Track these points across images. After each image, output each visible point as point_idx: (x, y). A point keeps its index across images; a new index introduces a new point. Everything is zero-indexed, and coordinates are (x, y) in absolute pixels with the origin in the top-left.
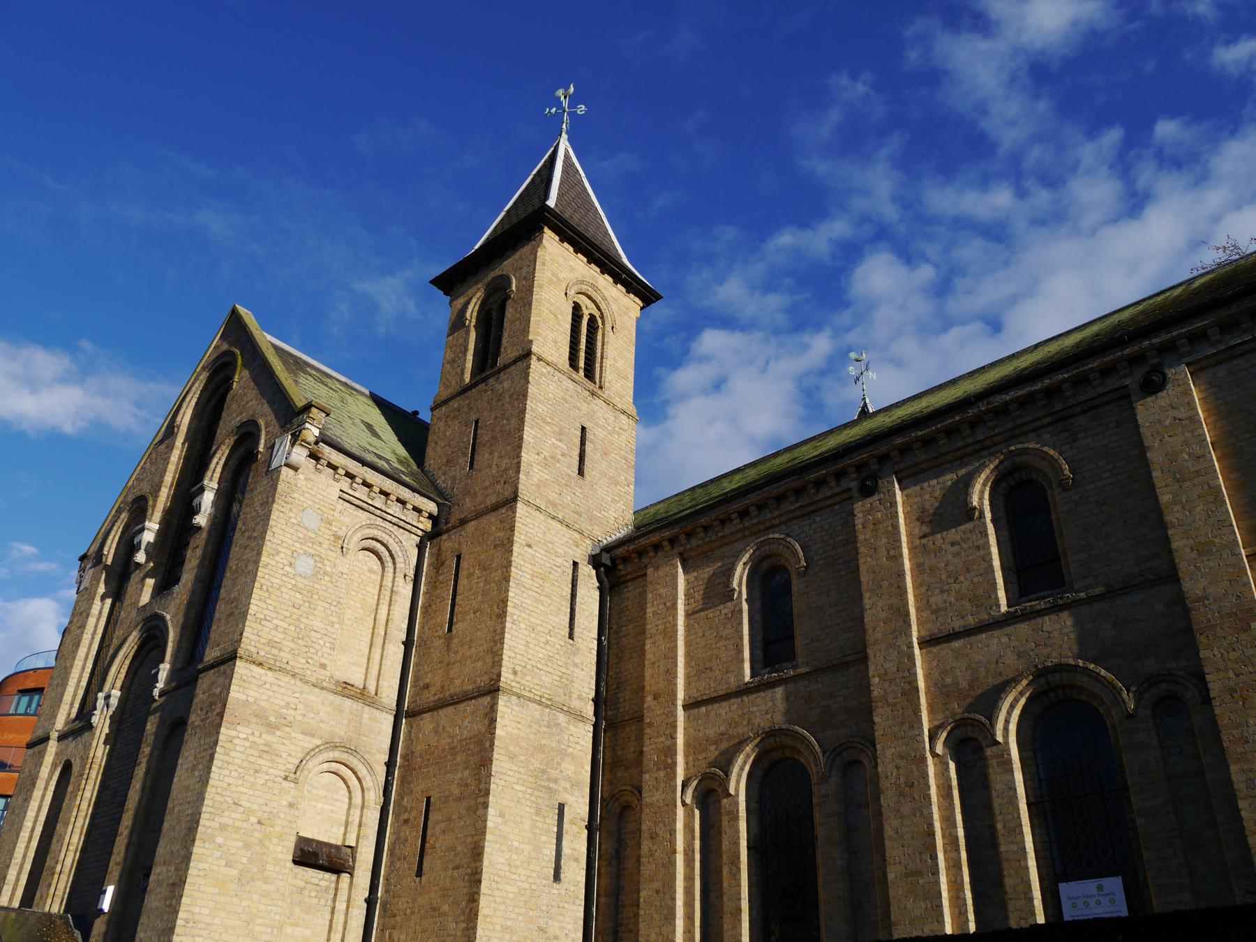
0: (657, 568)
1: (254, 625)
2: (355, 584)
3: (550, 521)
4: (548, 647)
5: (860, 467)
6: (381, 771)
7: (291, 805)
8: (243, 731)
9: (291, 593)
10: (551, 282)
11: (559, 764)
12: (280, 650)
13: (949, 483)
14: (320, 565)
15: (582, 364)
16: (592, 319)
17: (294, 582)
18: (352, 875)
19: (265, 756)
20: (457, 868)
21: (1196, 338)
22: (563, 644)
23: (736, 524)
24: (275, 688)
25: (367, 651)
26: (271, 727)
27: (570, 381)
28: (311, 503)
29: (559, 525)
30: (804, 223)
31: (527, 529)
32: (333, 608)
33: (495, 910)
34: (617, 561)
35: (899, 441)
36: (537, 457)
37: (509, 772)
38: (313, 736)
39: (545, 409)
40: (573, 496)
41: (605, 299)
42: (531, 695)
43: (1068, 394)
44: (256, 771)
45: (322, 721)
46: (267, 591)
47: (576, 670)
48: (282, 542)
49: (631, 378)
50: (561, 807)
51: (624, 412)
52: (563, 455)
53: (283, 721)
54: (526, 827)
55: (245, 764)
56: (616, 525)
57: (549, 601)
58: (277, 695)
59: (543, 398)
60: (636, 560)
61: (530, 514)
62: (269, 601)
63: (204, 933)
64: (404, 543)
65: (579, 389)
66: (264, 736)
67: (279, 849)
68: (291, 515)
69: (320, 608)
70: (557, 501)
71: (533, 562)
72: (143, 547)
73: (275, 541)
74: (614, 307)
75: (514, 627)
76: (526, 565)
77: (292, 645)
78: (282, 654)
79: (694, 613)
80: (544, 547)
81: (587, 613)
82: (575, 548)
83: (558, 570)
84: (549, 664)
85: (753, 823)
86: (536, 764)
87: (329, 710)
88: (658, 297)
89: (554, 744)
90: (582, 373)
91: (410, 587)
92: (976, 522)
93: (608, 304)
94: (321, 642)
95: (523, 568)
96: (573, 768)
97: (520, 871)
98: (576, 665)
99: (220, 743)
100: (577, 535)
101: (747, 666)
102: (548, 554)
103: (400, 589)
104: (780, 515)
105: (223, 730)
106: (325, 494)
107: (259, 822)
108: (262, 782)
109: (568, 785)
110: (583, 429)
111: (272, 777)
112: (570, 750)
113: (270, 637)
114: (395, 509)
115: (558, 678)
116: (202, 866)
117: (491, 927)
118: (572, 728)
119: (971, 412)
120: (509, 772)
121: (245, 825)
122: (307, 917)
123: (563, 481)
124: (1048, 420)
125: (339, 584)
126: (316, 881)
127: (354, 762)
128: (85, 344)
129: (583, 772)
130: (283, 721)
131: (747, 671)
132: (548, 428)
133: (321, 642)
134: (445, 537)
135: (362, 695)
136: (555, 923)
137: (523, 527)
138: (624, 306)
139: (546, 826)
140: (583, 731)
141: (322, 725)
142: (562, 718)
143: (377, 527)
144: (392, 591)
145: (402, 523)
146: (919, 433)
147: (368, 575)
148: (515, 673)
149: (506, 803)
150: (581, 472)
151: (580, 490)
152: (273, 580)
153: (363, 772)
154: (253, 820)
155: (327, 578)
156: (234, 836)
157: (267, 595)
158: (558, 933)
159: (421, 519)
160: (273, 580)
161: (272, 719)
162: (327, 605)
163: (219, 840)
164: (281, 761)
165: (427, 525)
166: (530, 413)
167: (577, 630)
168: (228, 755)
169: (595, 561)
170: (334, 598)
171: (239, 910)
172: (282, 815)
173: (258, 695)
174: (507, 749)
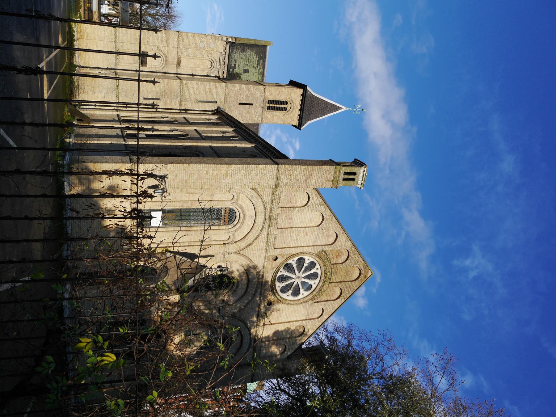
3: (224, 94)
7: (152, 49)
8: (164, 35)
10: (288, 92)
15: (271, 105)
26: (166, 42)
29: (224, 97)
38: (167, 53)
41: (292, 111)
51: (262, 119)
52: (242, 98)
65: (262, 103)
74: (291, 115)
87: (173, 56)
88: (300, 129)
89: (173, 97)
90: (268, 105)
91: (206, 75)
96: (169, 103)
97: (145, 88)
98: (192, 103)
100: (223, 103)
107: (148, 41)
109: (165, 101)
110: (252, 104)
114: (222, 67)
118: (177, 102)
127: (164, 64)
128: (415, 129)
135: (179, 64)
142: (179, 99)
143: (217, 64)
148: (186, 84)
150: (240, 104)
158: (134, 99)
167: (200, 103)
169: (219, 108)
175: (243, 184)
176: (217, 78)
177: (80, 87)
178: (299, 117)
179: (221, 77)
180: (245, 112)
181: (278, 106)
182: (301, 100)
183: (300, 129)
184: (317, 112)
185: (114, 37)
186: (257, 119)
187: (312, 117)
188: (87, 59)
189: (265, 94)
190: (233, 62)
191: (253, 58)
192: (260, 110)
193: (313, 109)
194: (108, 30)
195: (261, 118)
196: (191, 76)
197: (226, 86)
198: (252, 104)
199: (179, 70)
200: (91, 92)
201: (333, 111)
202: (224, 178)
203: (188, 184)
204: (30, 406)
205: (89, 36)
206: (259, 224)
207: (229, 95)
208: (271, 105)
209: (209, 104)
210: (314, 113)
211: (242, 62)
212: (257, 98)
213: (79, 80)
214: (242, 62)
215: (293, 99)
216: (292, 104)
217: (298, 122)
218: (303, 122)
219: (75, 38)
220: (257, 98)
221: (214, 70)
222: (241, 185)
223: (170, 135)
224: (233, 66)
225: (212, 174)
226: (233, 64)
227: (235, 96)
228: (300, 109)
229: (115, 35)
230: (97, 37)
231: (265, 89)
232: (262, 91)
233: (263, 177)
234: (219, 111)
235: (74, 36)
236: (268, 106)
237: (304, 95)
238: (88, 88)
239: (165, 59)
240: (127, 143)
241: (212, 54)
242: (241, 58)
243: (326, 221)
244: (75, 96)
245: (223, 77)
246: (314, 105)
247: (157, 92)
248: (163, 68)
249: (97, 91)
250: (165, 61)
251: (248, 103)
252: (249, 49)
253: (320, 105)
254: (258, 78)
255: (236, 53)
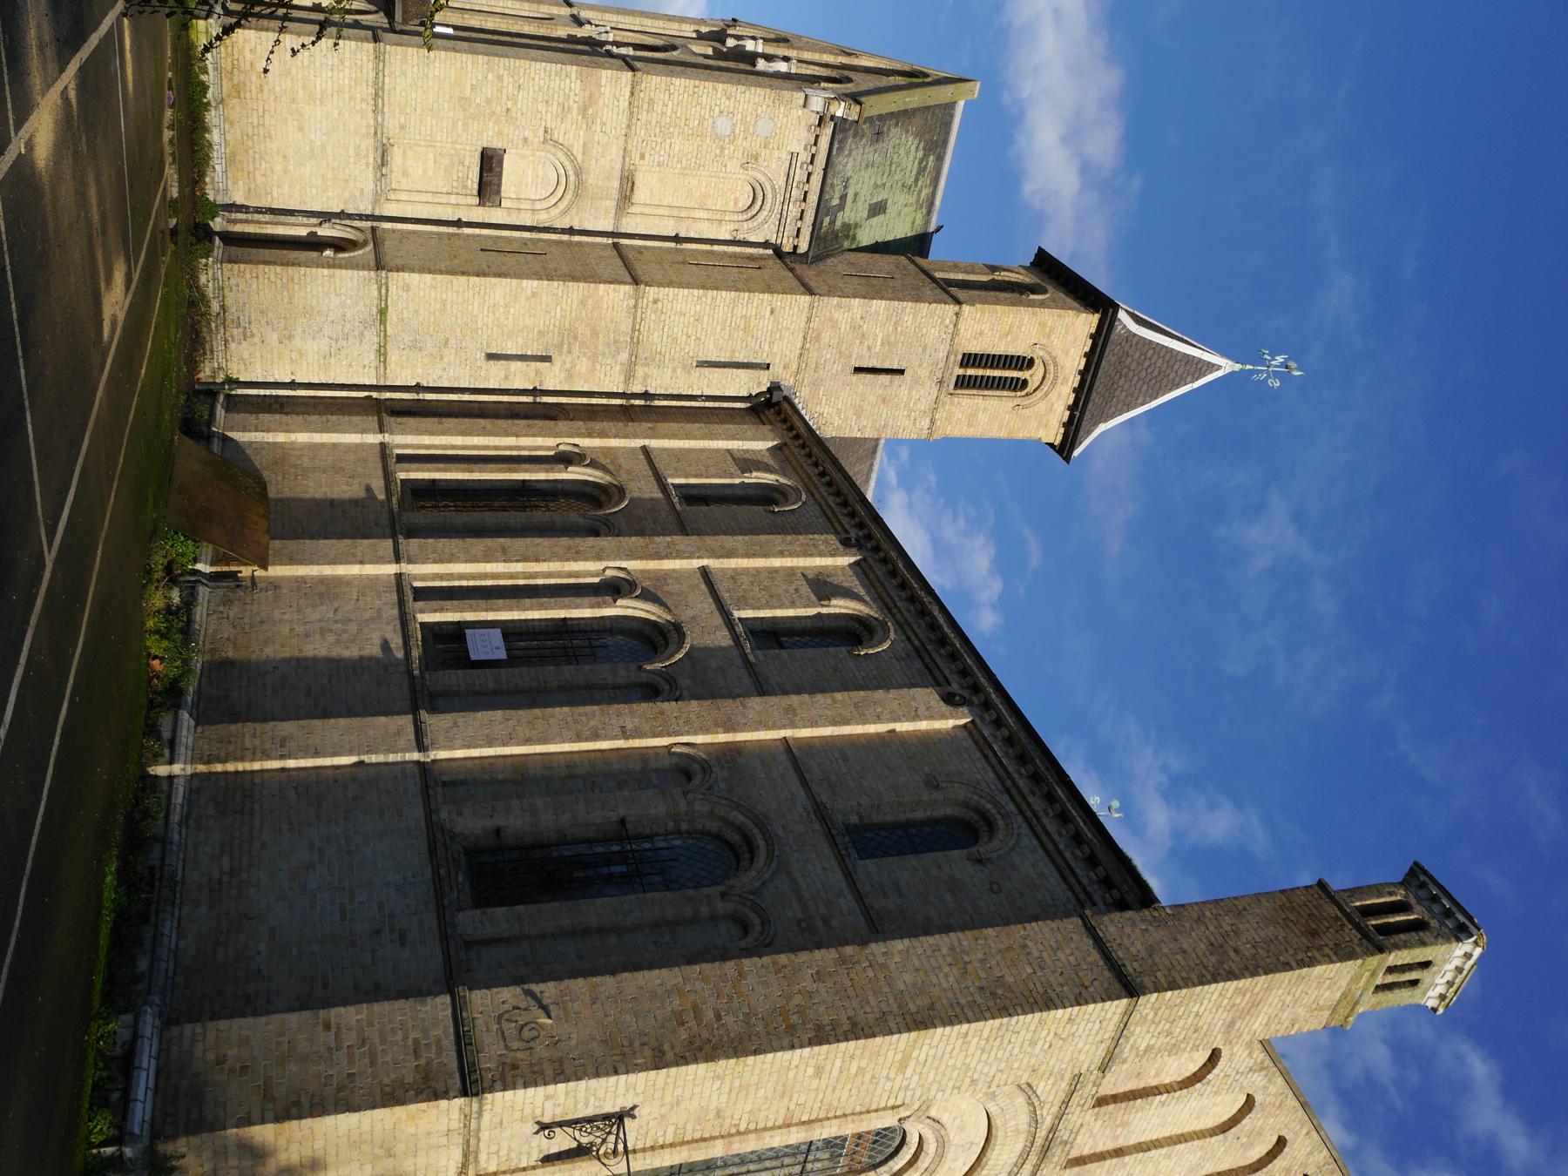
0: (771, 431)
1: (663, 85)
2: (721, 185)
3: (801, 335)
4: (684, 337)
5: (869, 537)
6: (564, 223)
7: (525, 140)
8: (577, 86)
9: (697, 116)
10: (1043, 325)
11: (585, 354)
12: (648, 111)
13: (856, 590)
14: (727, 141)
15: (971, 372)
16: (1025, 383)
17: (707, 116)
18: (479, 205)
19: (560, 108)
20: (489, 267)
21: (998, 723)
22: (691, 354)
23: (813, 471)
24: (616, 111)
25: (665, 204)
26: (584, 111)
27: (946, 353)
28: (779, 125)
30: (1512, 1091)
31: (787, 308)
32: (693, 160)
33: (458, 292)
34: (777, 408)
35: (893, 554)
36: (859, 317)
37: (570, 300)
38: (584, 154)
39: (909, 324)
40: (832, 361)
41: (1046, 395)
42: (638, 320)
43: (942, 651)
44: (547, 102)
45: (597, 160)
46: (694, 93)
47: (670, 370)
48: (739, 102)
49: (970, 433)
50: (546, 359)
51: (933, 422)
52: (869, 348)
53: (590, 121)
54: (527, 321)
55: (551, 91)
56: (816, 415)
57: (726, 337)
58: (610, 113)
59: (919, 320)
60: (778, 419)
61: (802, 311)
62: (686, 96)
63: (421, 74)
64: (766, 226)
65: (941, 365)
66: (576, 105)
67: (491, 133)
68: (764, 107)
69: (691, 147)
70: (822, 343)
71: (758, 316)
72: (740, 43)
73: (738, 95)
74: (1042, 406)
75: (695, 299)
76: (754, 309)
77: (654, 123)
78: (645, 113)
79: (731, 454)
80: (775, 329)
81: (724, 382)
82: (782, 365)
83: (757, 347)
84: (670, 339)
85: (545, 486)
86: (581, 329)
88: (1067, 459)
90: (961, 372)
91: (728, 237)
92: (817, 602)
93: (1042, 399)
94: (662, 152)
95: (750, 306)
96: (583, 370)
97: (491, 318)
98: (674, 371)
99: (564, 67)
100: (794, 367)
101: (682, 481)
102: (769, 333)
103: (724, 227)
104: (823, 497)
105: (575, 67)
106: (791, 137)
107: (508, 110)
108: (540, 108)
109: (568, 365)
110: (901, 372)
111: (544, 117)
112: (598, 367)
113: (656, 100)
114: (794, 211)
115: (659, 350)
116: (469, 64)
117: (444, 288)
118: (618, 368)
119: (922, 594)
120: (570, 300)
121: (504, 97)
122: (442, 170)
123: (843, 349)
124: (917, 643)
125: (715, 164)
126: (470, 177)
127: (568, 196)
129: (582, 382)
130: (590, 121)
131: (677, 481)
132: (891, 328)
133: (662, 152)
134: (778, 261)
136: (452, 357)
137: (788, 304)
138: (1048, 421)
139: (530, 342)
140: (616, 381)
141: (593, 162)
142: (624, 356)
143: (774, 197)
144: (721, 221)
145: (783, 221)
146: (901, 565)
147: (732, 198)
148: (655, 301)
149: (544, 299)
150: (858, 370)
151: (839, 369)
152: (705, 96)
153: (562, 205)
154: (509, 104)
155: (718, 151)
156: (495, 89)
157: (691, 93)
158: (446, 360)
159: (791, 239)
160: (705, 96)
161: (590, 111)
162: (695, 154)
163: (490, 76)
164: (559, 123)
165: (787, 248)
166: (900, 307)
167: (706, 371)
168: (556, 75)
169: (775, 388)
170: (703, 160)
171: (441, 101)
172: (516, 133)
173: (607, 95)
174: (589, 297)
175: (968, 1081)
176: (770, 252)
177: (229, 318)
178: (1068, 413)
179: (787, 248)
180: (872, 399)
181: (997, 373)
182: (1086, 355)
183: (1067, 459)
184: (1132, 389)
185: (371, 90)
186: (914, 423)
187: (1113, 410)
188: (260, 180)
189: (955, 334)
190: (837, 189)
191: (908, 153)
192: (929, 392)
193: (1122, 382)
194: (347, 64)
195: (928, 421)
196: (673, 245)
197: (811, 307)
198: (901, 372)
199: (624, 221)
200: (276, 337)
201: (1189, 379)
202: (892, 1076)
203: (728, 1121)
204: (99, 1152)
205: (266, 88)
206: (999, 1168)
207: (818, 338)
208: (971, 372)
209: (740, 371)
210: (1124, 394)
211: (867, 180)
212: (924, 350)
213: (226, 290)
214: (867, 180)
215: (1058, 353)
216: (1051, 368)
217: (1062, 430)
218: (1081, 433)
219: (209, 95)
220: (924, 350)
221: (760, 218)
222: (957, 1084)
223: (602, 618)
224: (835, 202)
225: (841, 1072)
226: (837, 195)
227: (841, 341)
228: (1076, 385)
229: (376, 83)
230: (301, 91)
231: (957, 314)
232: (947, 321)
233: (1058, 1046)
234: (775, 399)
235: (204, 88)
236: (958, 376)
237: (1101, 339)
238: (263, 321)
239: (572, 178)
240: (432, 757)
241: (760, 160)
242: (867, 166)
243: (1258, 1113)
244: (212, 352)
245: (795, 247)
246: (1129, 367)
247: (540, 332)
248: (564, 212)
249: (299, 330)
250: (571, 186)
251: (886, 366)
252: (897, 125)
253: (1147, 363)
254: (913, 223)
255: (851, 151)
